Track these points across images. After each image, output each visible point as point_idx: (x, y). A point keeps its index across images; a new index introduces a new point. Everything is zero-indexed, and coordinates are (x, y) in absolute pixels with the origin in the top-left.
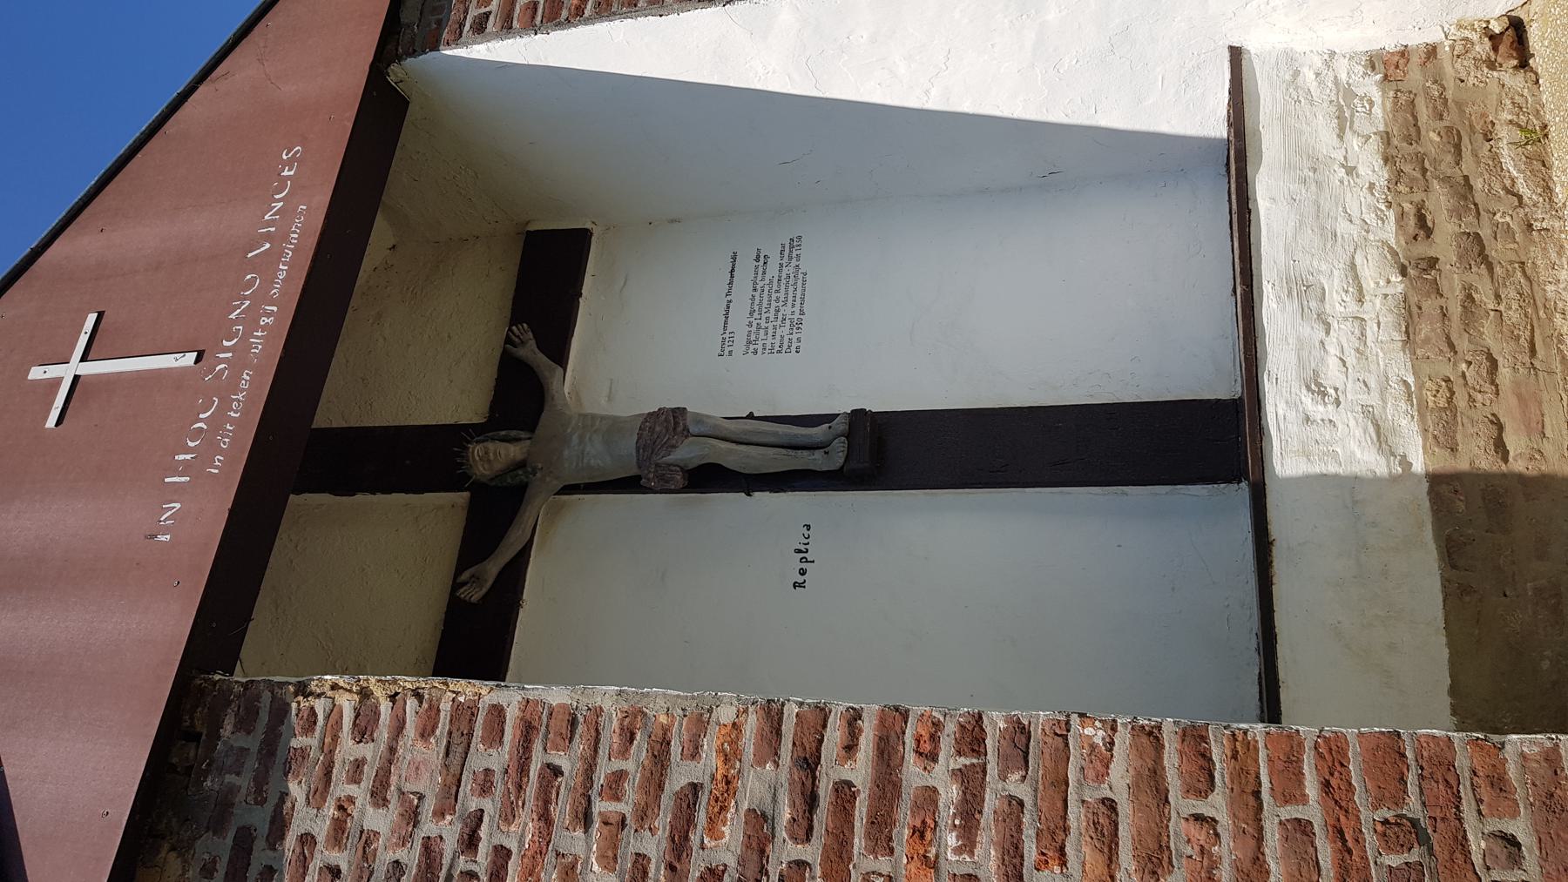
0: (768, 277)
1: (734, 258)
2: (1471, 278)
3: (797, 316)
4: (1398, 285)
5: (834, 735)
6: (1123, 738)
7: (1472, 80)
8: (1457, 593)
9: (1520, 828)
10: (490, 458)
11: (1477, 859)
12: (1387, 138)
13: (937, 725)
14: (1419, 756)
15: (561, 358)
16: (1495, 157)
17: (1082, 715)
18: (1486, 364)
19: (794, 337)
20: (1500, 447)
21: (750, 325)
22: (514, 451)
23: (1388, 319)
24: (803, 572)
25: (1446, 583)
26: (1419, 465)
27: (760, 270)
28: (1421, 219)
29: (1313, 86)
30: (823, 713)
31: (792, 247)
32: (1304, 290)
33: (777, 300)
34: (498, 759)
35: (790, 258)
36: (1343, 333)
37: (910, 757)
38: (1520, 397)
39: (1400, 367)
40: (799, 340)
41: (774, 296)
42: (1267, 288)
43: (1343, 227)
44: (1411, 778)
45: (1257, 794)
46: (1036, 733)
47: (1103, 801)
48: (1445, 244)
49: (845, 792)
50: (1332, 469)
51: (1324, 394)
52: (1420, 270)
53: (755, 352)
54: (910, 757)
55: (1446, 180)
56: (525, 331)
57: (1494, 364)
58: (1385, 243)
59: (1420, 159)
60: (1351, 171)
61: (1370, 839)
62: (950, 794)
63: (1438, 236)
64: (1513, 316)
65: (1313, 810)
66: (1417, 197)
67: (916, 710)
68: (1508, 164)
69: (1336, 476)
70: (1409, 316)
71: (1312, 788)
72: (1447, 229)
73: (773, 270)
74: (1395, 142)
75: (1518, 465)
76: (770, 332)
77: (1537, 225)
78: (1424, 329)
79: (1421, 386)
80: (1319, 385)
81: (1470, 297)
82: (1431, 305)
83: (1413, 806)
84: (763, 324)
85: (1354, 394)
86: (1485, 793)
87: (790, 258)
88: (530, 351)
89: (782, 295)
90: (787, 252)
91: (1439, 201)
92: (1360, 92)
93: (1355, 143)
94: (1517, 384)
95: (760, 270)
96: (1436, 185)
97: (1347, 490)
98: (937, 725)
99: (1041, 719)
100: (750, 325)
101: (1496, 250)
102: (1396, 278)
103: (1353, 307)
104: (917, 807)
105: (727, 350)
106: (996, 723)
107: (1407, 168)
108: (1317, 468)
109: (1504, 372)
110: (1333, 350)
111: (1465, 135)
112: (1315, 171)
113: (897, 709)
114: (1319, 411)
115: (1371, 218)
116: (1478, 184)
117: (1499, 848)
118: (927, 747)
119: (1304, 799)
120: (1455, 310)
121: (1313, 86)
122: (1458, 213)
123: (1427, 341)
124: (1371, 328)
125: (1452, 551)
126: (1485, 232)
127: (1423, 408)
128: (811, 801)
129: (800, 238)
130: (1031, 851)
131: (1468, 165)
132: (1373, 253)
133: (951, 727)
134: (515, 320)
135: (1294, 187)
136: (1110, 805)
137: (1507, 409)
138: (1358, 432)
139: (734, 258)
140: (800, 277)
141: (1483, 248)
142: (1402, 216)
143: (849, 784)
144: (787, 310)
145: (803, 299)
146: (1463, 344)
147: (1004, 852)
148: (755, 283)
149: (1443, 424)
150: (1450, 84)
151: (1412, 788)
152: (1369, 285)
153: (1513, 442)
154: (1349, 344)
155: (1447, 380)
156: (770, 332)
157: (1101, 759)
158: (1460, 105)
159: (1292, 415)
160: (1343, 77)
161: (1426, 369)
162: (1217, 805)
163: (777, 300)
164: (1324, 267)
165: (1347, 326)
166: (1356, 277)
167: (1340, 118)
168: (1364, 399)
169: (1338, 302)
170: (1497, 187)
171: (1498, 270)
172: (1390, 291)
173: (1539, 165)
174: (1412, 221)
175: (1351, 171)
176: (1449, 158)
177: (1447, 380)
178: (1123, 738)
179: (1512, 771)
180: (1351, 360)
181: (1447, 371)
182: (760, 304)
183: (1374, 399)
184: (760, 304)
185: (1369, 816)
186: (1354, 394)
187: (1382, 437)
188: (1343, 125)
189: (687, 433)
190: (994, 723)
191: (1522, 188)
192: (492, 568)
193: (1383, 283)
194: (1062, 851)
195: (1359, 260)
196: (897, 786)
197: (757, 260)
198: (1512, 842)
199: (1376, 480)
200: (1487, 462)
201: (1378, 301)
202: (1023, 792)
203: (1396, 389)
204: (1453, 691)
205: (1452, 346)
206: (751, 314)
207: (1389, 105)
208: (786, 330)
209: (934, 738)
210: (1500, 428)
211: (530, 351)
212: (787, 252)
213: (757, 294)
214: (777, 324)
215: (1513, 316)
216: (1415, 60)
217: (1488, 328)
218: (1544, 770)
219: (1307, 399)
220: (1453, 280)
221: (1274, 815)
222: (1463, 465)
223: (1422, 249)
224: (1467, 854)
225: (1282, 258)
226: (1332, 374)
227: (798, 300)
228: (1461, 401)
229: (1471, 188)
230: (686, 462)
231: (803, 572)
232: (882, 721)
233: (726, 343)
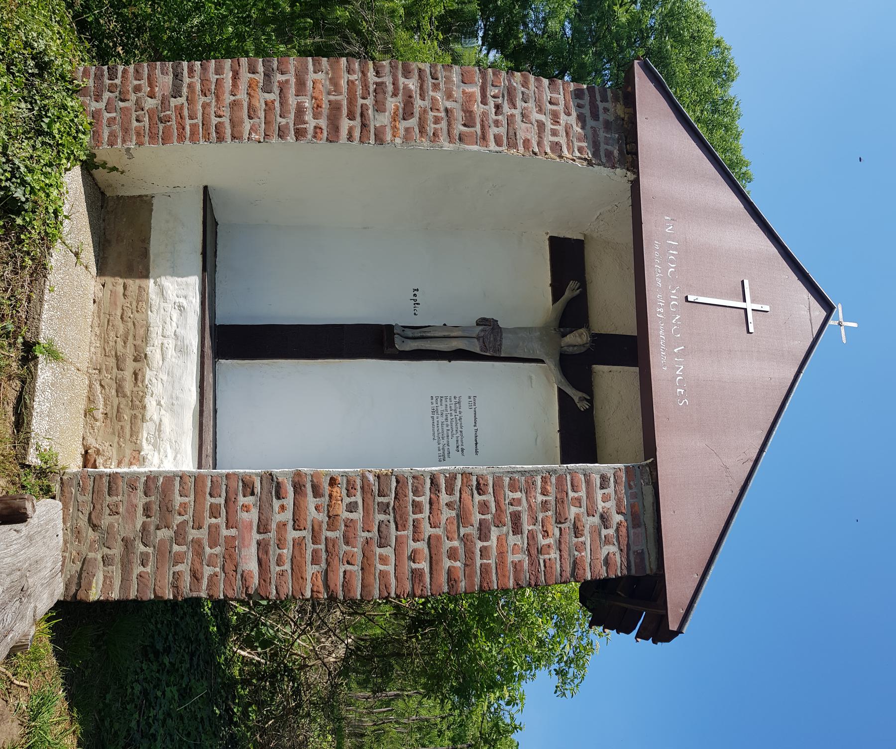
0: (455, 439)
1: (477, 452)
2: (123, 351)
3: (435, 416)
4: (148, 350)
5: (357, 134)
6: (246, 136)
7: (107, 444)
8: (145, 240)
9: (135, 124)
10: (577, 339)
11: (147, 115)
12: (143, 419)
13: (315, 137)
14: (158, 140)
15: (562, 394)
16: (105, 405)
17: (260, 142)
18: (125, 319)
19: (435, 405)
20: (125, 287)
21: (460, 412)
22: (571, 339)
23: (154, 335)
24: (415, 295)
25: (149, 243)
26: (152, 281)
27: (460, 443)
28: (136, 379)
29: (169, 451)
30: (361, 141)
31: (444, 455)
32: (182, 350)
33: (447, 426)
34: (493, 131)
35: (443, 449)
36: (170, 331)
37: (324, 127)
38: (116, 304)
39: (153, 317)
40: (432, 403)
41: (449, 428)
42: (195, 351)
43: (165, 378)
44: (161, 133)
45: (203, 125)
46: (276, 136)
47: (252, 118)
48: (130, 365)
49: (351, 117)
50: (179, 279)
51: (179, 306)
52: (140, 357)
53: (455, 398)
54: (324, 127)
55: (125, 396)
56: (583, 406)
57: (122, 318)
58: (151, 370)
59: (133, 407)
60: (159, 404)
61: (174, 118)
62: (309, 117)
63: (132, 370)
64: (112, 334)
65: (188, 122)
66: (136, 389)
67: (324, 141)
68: (101, 400)
69: (179, 277)
70: (146, 339)
71: (188, 128)
72: (128, 374)
73: (453, 442)
74: (140, 416)
75: (121, 281)
76: (449, 409)
77: (97, 372)
78: (142, 332)
79: (146, 310)
80: (180, 310)
81: (125, 343)
82: (138, 342)
83: (161, 126)
84: (453, 412)
85: (169, 307)
86: (142, 132)
87: (443, 449)
88: (575, 395)
89: (445, 428)
90: (446, 452)
91: (128, 387)
92: (151, 447)
93: (156, 417)
94: (116, 309)
95: (460, 443)
96: (129, 394)
97: (176, 271)
98: (315, 137)
99: (275, 140)
100: (460, 412)
101: (112, 362)
102: (149, 353)
103: (165, 342)
104: (320, 113)
105: (472, 399)
106: (291, 138)
107: (138, 403)
108: (184, 279)
109: (119, 313)
110: (174, 324)
111: (114, 416)
112: (173, 404)
113: (331, 142)
114: (182, 300)
115: (154, 380)
116: (114, 392)
117: (141, 118)
118: (318, 130)
119: (190, 125)
120: (130, 338)
121: (169, 451)
122: (124, 379)
123: (142, 327)
124: (160, 333)
125: (145, 254)
126: (115, 370)
127: (147, 302)
128: (362, 115)
129: (440, 461)
130: (277, 104)
131: (116, 401)
132: (155, 365)
133: (309, 137)
134: (590, 413)
135: (181, 396)
136: (250, 118)
137: (121, 300)
138: (169, 292)
139: (477, 452)
140: (438, 436)
141: (117, 364)
142: (143, 381)
143: (350, 119)
144: (441, 419)
145: (433, 425)
146: (130, 325)
147: (287, 101)
148: (462, 436)
149: (142, 297)
150: (115, 445)
151: (161, 131)
152: (159, 351)
153: (120, 289)
154: (168, 326)
155: (138, 311)
156: (449, 409)
157: (252, 129)
158: (114, 433)
159: (191, 298)
160: (156, 454)
161: (144, 316)
162: (215, 121)
163: (447, 426)
164: (174, 360)
165: (168, 333)
166: (163, 355)
167: (160, 431)
168: (165, 305)
169: (170, 344)
170: (107, 390)
171: (113, 353)
172: (152, 348)
173: (91, 400)
174: (139, 377)
175: (159, 404)
176: (122, 406)
177: (138, 311)
178: (246, 136)
179: (134, 138)
180: (168, 319)
181: (137, 315)
182: (457, 424)
183: (162, 305)
184: (457, 424)
185: (173, 123)
186: (169, 307)
187: (162, 291)
188: (159, 428)
189: (478, 338)
190: (292, 138)
191: (98, 387)
192: (568, 294)
193: (154, 352)
194: (266, 104)
195: (161, 362)
196: (329, 118)
197: (463, 450)
198: (137, 120)
199: (165, 275)
200: (130, 282)
201: (156, 344)
202: (279, 119)
203: (154, 309)
204: (152, 210)
205: (134, 324)
206: (460, 419)
207: (140, 435)
208: (440, 409)
209: (316, 133)
210: (124, 295)
211: (575, 395)
212: (446, 452)
213: (459, 429)
214: (446, 413)
215: (112, 334)
216: (127, 460)
217: (121, 331)
218: (126, 138)
219: (185, 304)
220: (130, 351)
221: (199, 120)
222: (138, 281)
223: (137, 365)
224: (149, 117)
225: (189, 364)
226: (175, 315)
227: (436, 423)
228: (134, 304)
229: (117, 391)
230: (486, 343)
231: (415, 295)
232: (338, 137)
233: (473, 401)
